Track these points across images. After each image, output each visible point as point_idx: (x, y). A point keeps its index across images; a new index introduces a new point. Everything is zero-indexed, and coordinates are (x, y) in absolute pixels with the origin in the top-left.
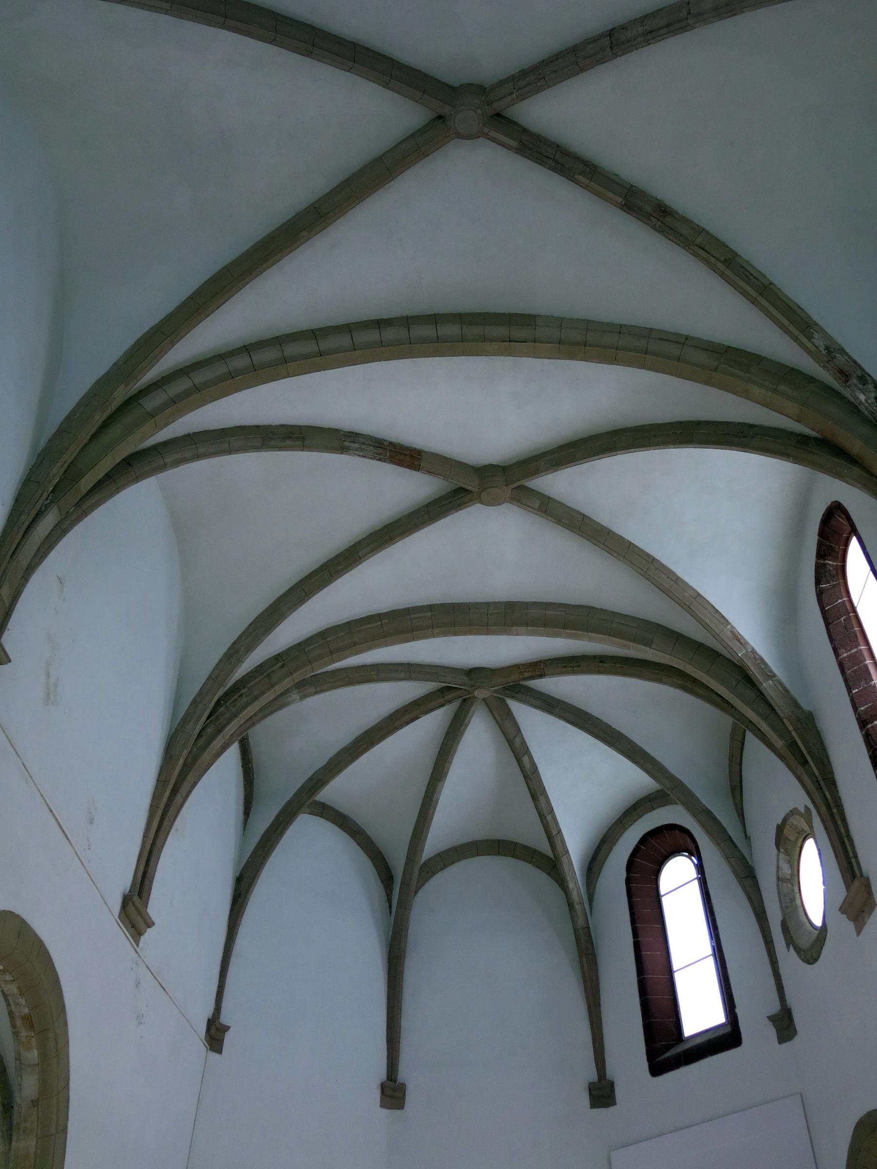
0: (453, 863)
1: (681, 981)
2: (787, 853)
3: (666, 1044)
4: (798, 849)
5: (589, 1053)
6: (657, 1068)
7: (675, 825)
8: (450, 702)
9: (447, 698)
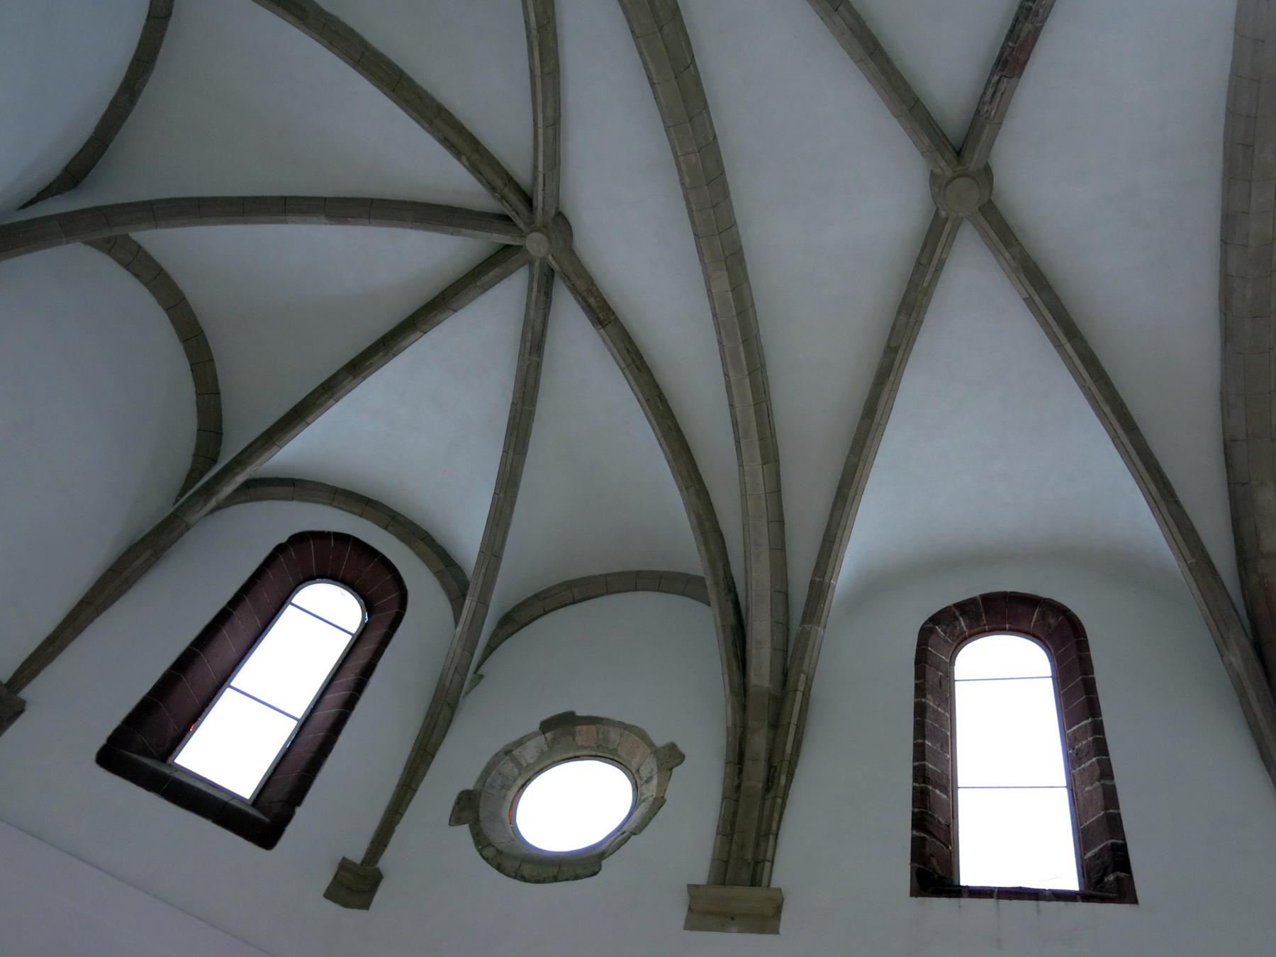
0: (137, 276)
2: (551, 745)
3: (142, 748)
4: (572, 755)
5: (29, 647)
8: (503, 198)
9: (506, 191)
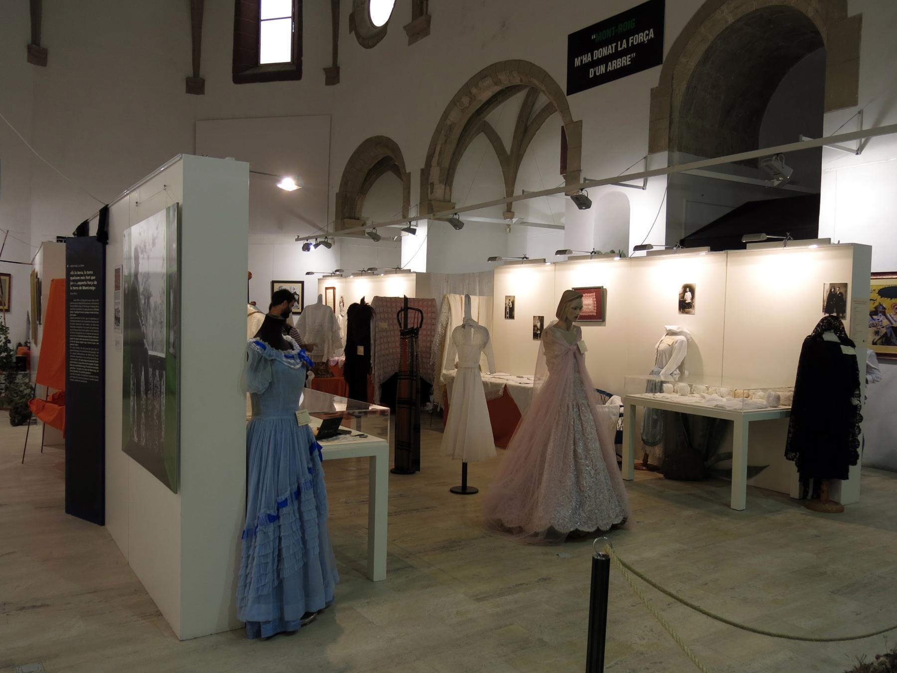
1: (266, 29)
6: (239, 77)
7: (494, 65)
